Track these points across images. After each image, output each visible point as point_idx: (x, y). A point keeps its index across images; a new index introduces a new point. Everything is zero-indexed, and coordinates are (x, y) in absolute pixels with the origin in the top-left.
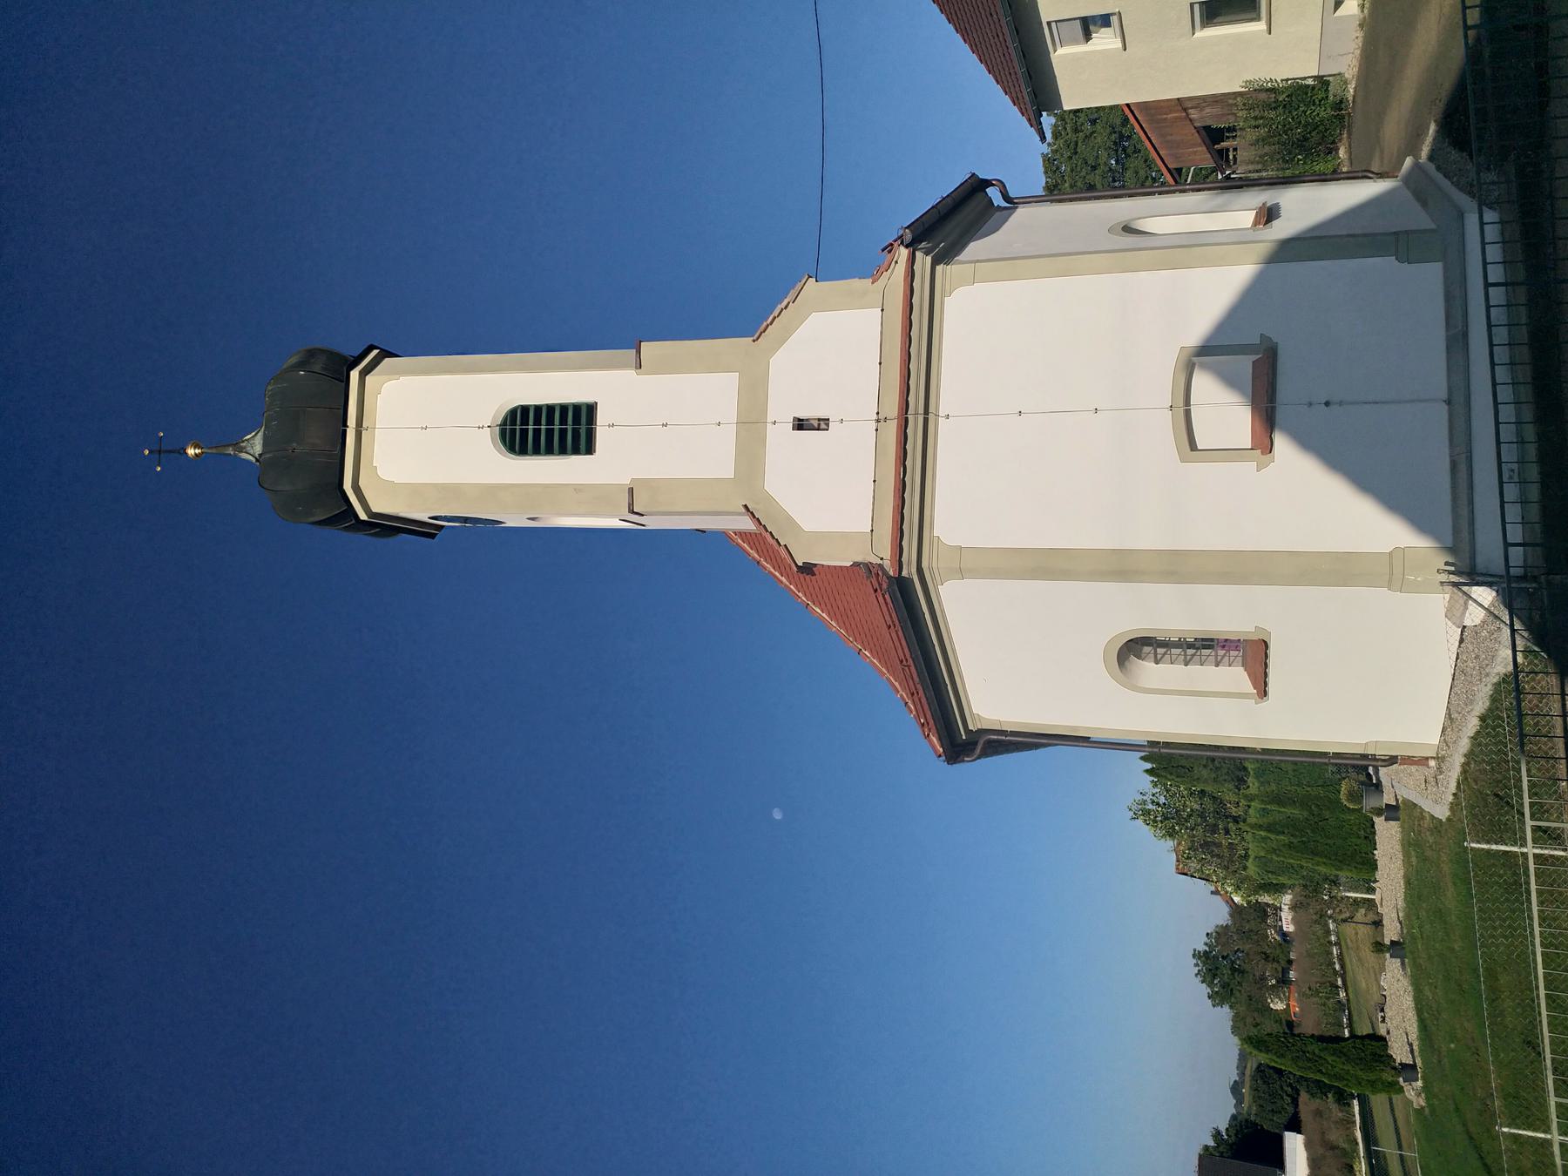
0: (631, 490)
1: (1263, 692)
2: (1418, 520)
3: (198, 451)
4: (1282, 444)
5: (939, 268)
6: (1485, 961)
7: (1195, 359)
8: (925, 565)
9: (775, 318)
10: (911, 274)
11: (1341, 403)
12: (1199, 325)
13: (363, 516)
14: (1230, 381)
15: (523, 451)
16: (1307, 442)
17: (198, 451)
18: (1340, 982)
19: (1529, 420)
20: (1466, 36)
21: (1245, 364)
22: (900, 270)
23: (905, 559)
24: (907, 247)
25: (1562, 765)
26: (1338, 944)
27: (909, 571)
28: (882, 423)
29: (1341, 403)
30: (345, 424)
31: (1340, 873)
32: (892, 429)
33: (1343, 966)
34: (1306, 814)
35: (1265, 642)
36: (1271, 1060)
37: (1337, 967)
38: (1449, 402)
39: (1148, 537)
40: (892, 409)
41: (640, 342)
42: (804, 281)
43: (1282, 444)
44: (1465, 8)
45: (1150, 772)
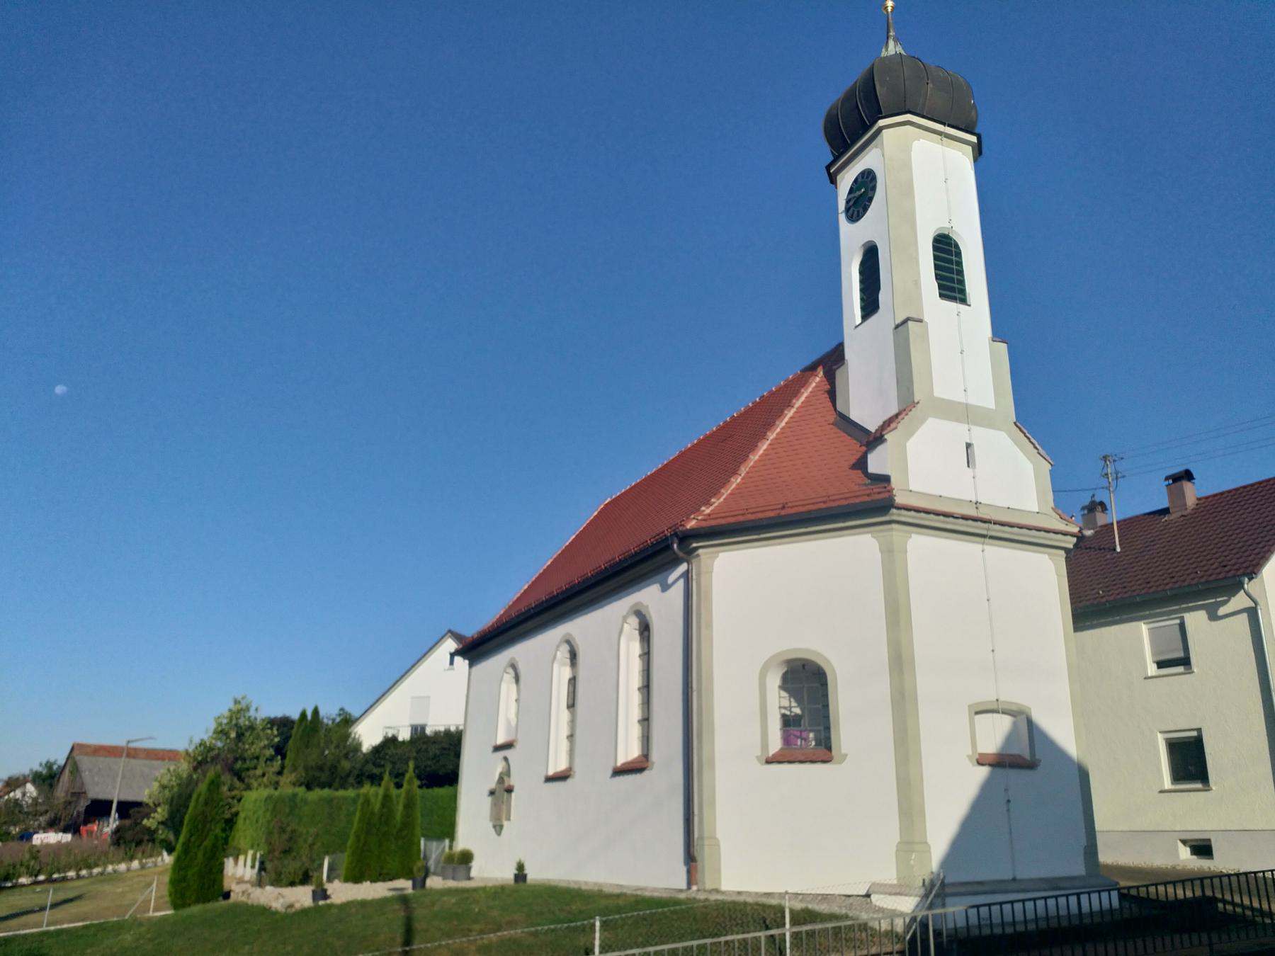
0: (921, 321)
1: (769, 762)
2: (947, 862)
3: (890, 9)
4: (984, 771)
5: (1062, 553)
6: (611, 920)
7: (1024, 717)
8: (894, 526)
9: (1029, 439)
10: (1065, 534)
11: (1008, 810)
12: (1045, 721)
13: (881, 123)
14: (1010, 738)
15: (935, 248)
16: (986, 788)
17: (890, 9)
18: (41, 878)
19: (1028, 928)
20: (1260, 872)
21: (1023, 750)
22: (1061, 526)
23: (903, 512)
24: (1080, 531)
25: (865, 952)
26: (91, 875)
27: (895, 514)
28: (975, 506)
29: (1008, 810)
30: (950, 126)
31: (346, 854)
32: (972, 512)
33: (55, 881)
34: (398, 826)
35: (831, 761)
36: (199, 795)
37: (55, 876)
38: (1014, 880)
39: (925, 682)
40: (983, 513)
41: (1007, 343)
42: (1050, 461)
43: (984, 771)
44: (1272, 871)
45: (303, 715)
